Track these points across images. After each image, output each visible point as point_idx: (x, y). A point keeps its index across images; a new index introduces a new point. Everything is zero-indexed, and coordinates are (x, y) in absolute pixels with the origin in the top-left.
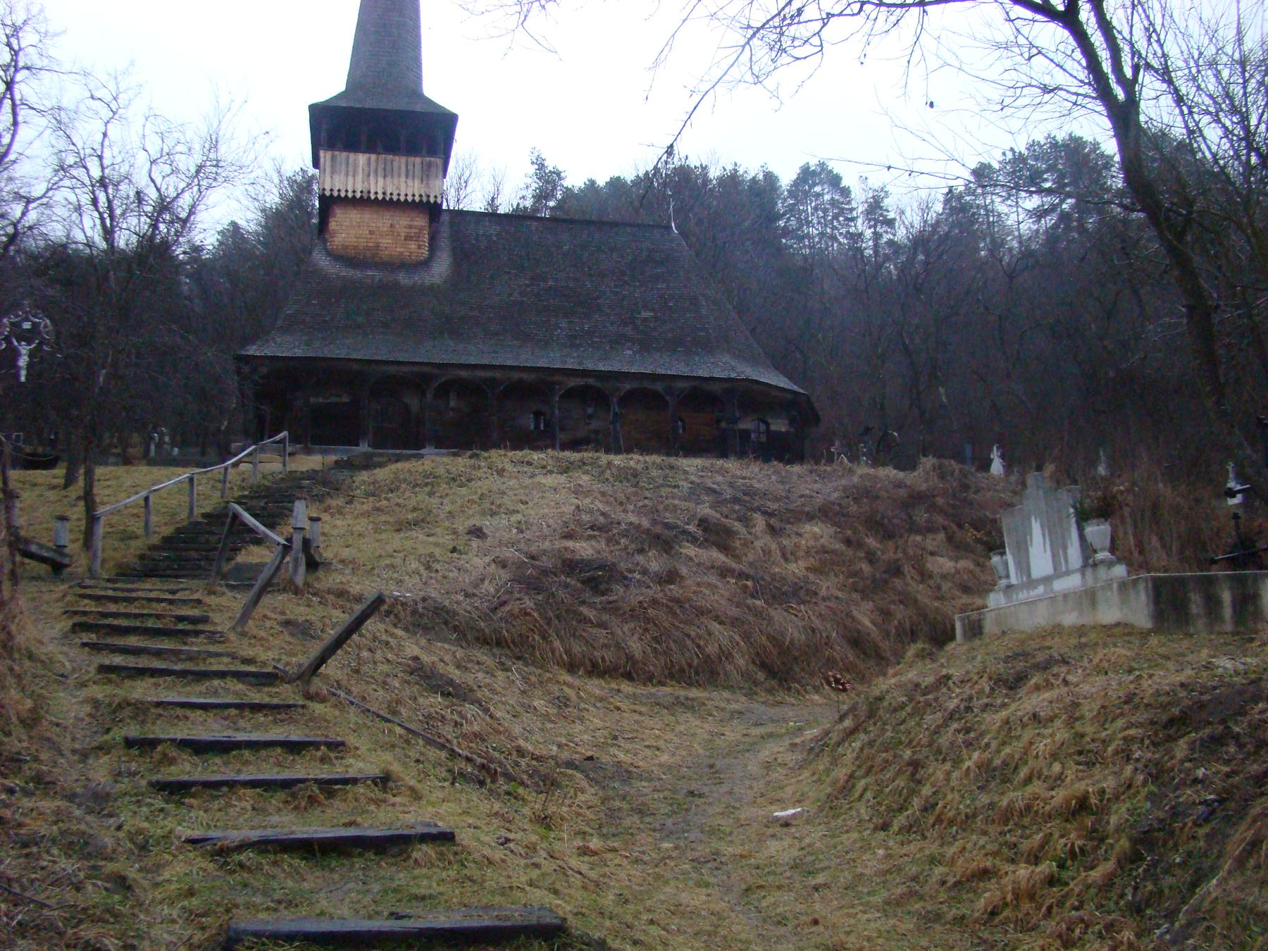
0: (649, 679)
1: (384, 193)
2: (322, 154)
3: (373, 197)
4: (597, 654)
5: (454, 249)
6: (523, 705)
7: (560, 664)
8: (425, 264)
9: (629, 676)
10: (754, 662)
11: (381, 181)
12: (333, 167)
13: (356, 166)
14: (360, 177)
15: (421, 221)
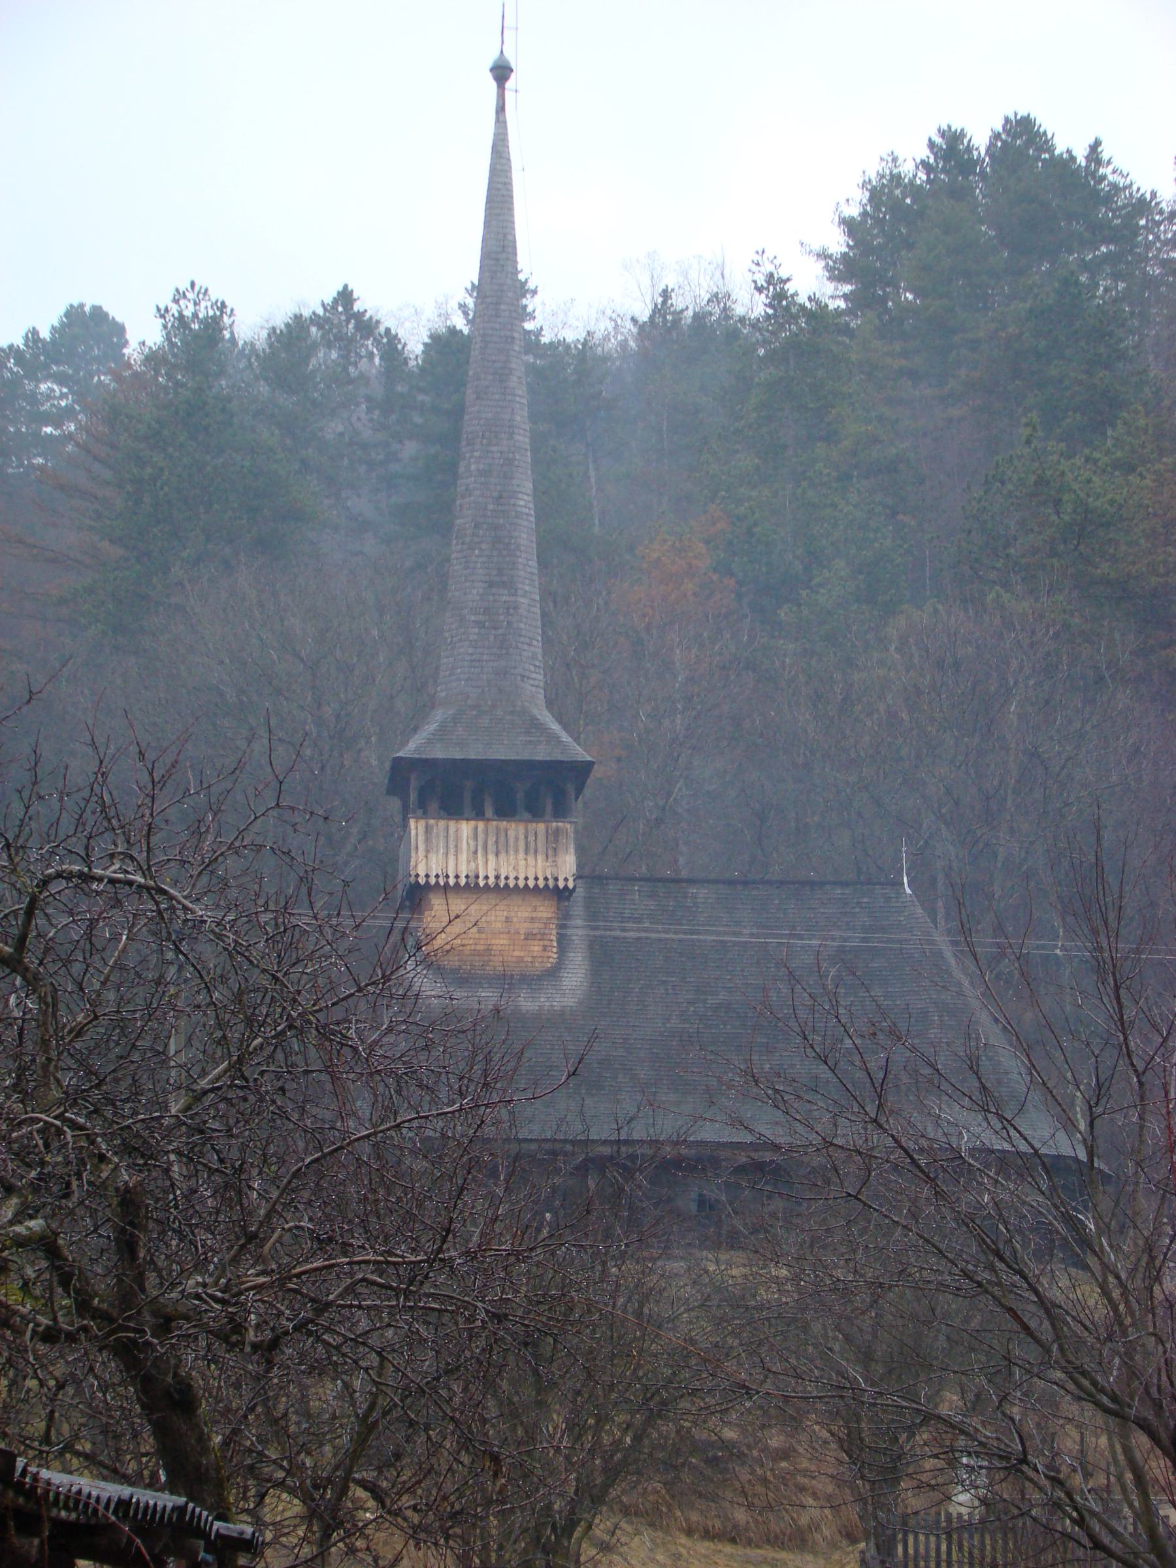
0: (749, 1543)
1: (497, 877)
2: (412, 823)
3: (482, 883)
4: (710, 1523)
5: (591, 947)
6: (649, 1558)
7: (681, 1529)
8: (553, 973)
9: (733, 1541)
10: (840, 1532)
11: (492, 857)
12: (427, 840)
13: (458, 839)
14: (463, 857)
15: (545, 910)
